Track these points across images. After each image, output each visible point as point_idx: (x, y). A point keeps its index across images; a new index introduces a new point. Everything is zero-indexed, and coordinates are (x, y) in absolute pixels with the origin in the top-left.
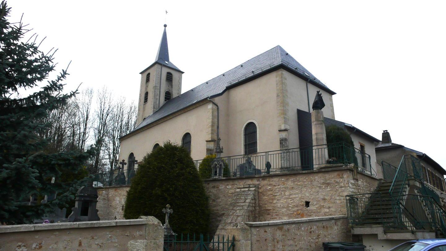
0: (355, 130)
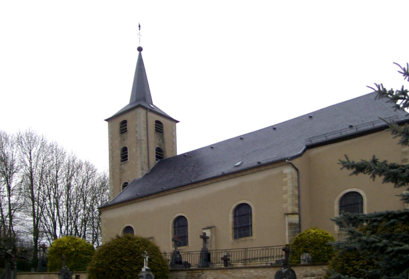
0: (238, 237)
